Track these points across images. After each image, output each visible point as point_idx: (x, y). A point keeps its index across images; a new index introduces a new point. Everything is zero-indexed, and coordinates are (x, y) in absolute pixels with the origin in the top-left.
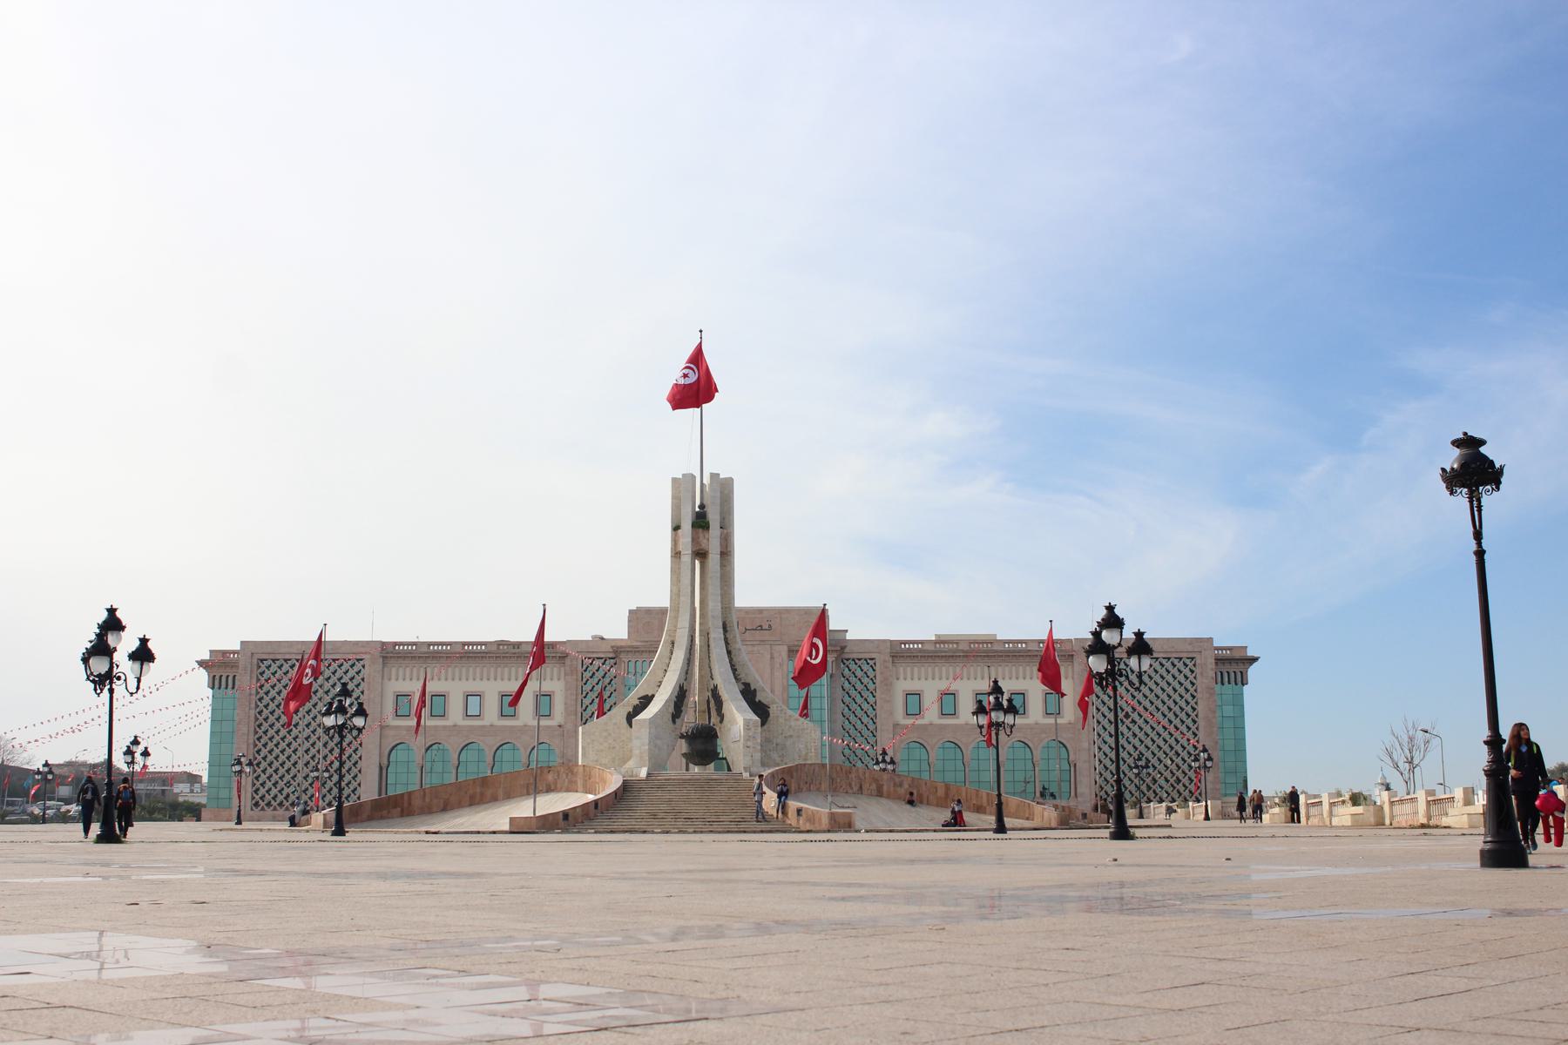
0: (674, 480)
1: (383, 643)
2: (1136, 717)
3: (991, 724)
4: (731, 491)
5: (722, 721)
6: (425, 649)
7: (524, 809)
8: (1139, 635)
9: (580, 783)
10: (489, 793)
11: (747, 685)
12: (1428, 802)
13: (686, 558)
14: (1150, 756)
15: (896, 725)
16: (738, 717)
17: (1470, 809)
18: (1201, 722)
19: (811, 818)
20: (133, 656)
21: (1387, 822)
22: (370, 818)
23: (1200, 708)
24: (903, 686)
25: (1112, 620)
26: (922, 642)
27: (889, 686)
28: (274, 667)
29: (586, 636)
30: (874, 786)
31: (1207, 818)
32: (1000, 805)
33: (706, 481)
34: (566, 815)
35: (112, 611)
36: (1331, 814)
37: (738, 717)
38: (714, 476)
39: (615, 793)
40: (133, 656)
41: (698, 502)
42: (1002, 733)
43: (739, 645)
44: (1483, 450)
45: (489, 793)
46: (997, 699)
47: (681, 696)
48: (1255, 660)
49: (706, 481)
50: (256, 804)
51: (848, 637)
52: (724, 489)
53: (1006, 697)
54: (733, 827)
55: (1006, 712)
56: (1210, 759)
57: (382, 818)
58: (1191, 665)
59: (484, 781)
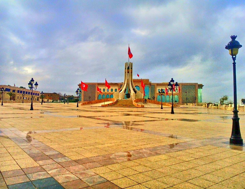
0: (125, 63)
1: (98, 83)
3: (161, 94)
4: (132, 64)
7: (103, 104)
8: (177, 83)
9: (112, 100)
11: (134, 89)
12: (225, 106)
13: (127, 73)
16: (132, 92)
17: (231, 108)
19: (139, 106)
20: (35, 85)
21: (219, 108)
22: (87, 104)
25: (172, 81)
26: (160, 83)
27: (156, 88)
28: (90, 85)
31: (195, 106)
32: (162, 104)
33: (129, 63)
34: (108, 105)
35: (32, 79)
36: (211, 107)
37: (132, 92)
38: (130, 62)
40: (35, 85)
41: (128, 66)
42: (162, 95)
44: (227, 45)
45: (102, 101)
46: (162, 91)
47: (125, 90)
48: (203, 86)
49: (129, 63)
51: (152, 83)
52: (132, 64)
54: (129, 107)
55: (163, 93)
56: (196, 98)
57: (89, 104)
59: (101, 100)
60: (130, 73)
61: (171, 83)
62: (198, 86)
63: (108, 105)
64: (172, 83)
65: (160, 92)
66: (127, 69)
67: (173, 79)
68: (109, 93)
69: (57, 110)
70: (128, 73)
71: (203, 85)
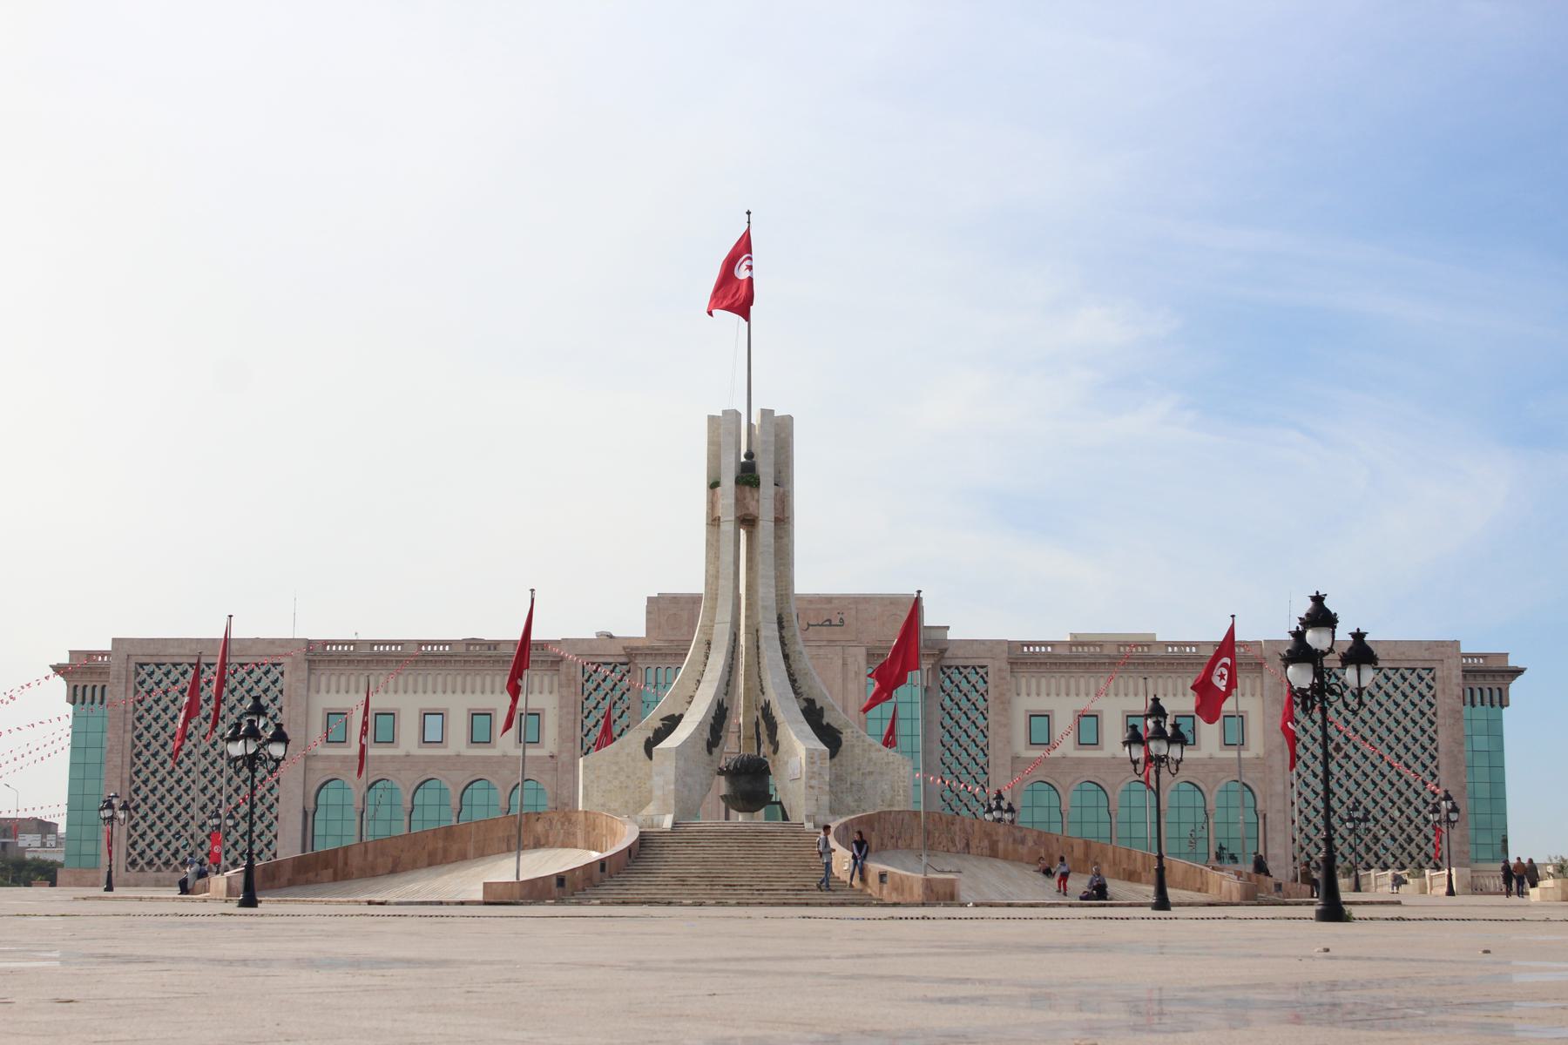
1: (310, 642)
2: (1351, 752)
5: (775, 751)
6: (413, 650)
7: (503, 870)
8: (1358, 636)
9: (580, 835)
10: (455, 848)
13: (728, 526)
14: (1370, 805)
15: (1015, 758)
16: (798, 747)
18: (1442, 758)
22: (291, 883)
23: (1441, 738)
24: (1026, 703)
25: (1321, 616)
27: (1006, 704)
28: (158, 675)
29: (591, 635)
30: (986, 843)
31: (1451, 892)
32: (1161, 871)
33: (756, 420)
34: (561, 879)
37: (798, 747)
38: (767, 414)
39: (629, 849)
41: (744, 450)
43: (800, 646)
45: (455, 848)
46: (1157, 723)
47: (719, 717)
49: (756, 420)
50: (133, 863)
51: (951, 635)
52: (780, 431)
53: (1169, 721)
55: (1170, 741)
56: (1455, 809)
57: (308, 882)
58: (1428, 679)
59: (448, 832)
60: (766, 526)
61: (1311, 636)
62: (1468, 672)
63: (561, 888)
64: (1315, 638)
65: (1135, 738)
66: (728, 482)
67: (1327, 603)
68: (458, 761)
69: (1283, 752)
70: (743, 532)
71: (1513, 662)
